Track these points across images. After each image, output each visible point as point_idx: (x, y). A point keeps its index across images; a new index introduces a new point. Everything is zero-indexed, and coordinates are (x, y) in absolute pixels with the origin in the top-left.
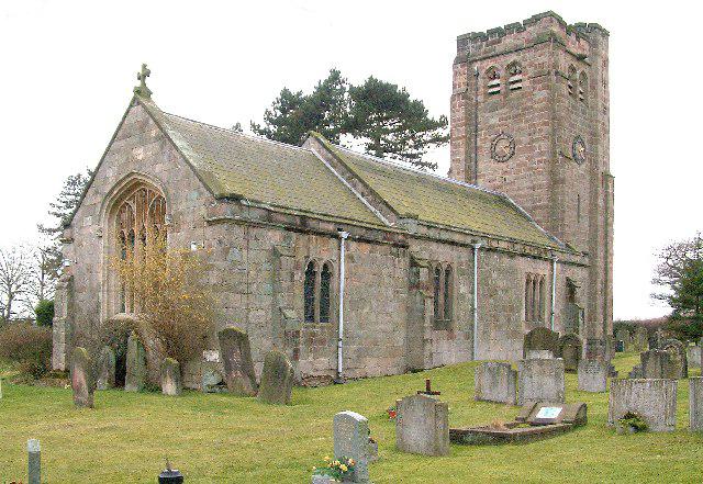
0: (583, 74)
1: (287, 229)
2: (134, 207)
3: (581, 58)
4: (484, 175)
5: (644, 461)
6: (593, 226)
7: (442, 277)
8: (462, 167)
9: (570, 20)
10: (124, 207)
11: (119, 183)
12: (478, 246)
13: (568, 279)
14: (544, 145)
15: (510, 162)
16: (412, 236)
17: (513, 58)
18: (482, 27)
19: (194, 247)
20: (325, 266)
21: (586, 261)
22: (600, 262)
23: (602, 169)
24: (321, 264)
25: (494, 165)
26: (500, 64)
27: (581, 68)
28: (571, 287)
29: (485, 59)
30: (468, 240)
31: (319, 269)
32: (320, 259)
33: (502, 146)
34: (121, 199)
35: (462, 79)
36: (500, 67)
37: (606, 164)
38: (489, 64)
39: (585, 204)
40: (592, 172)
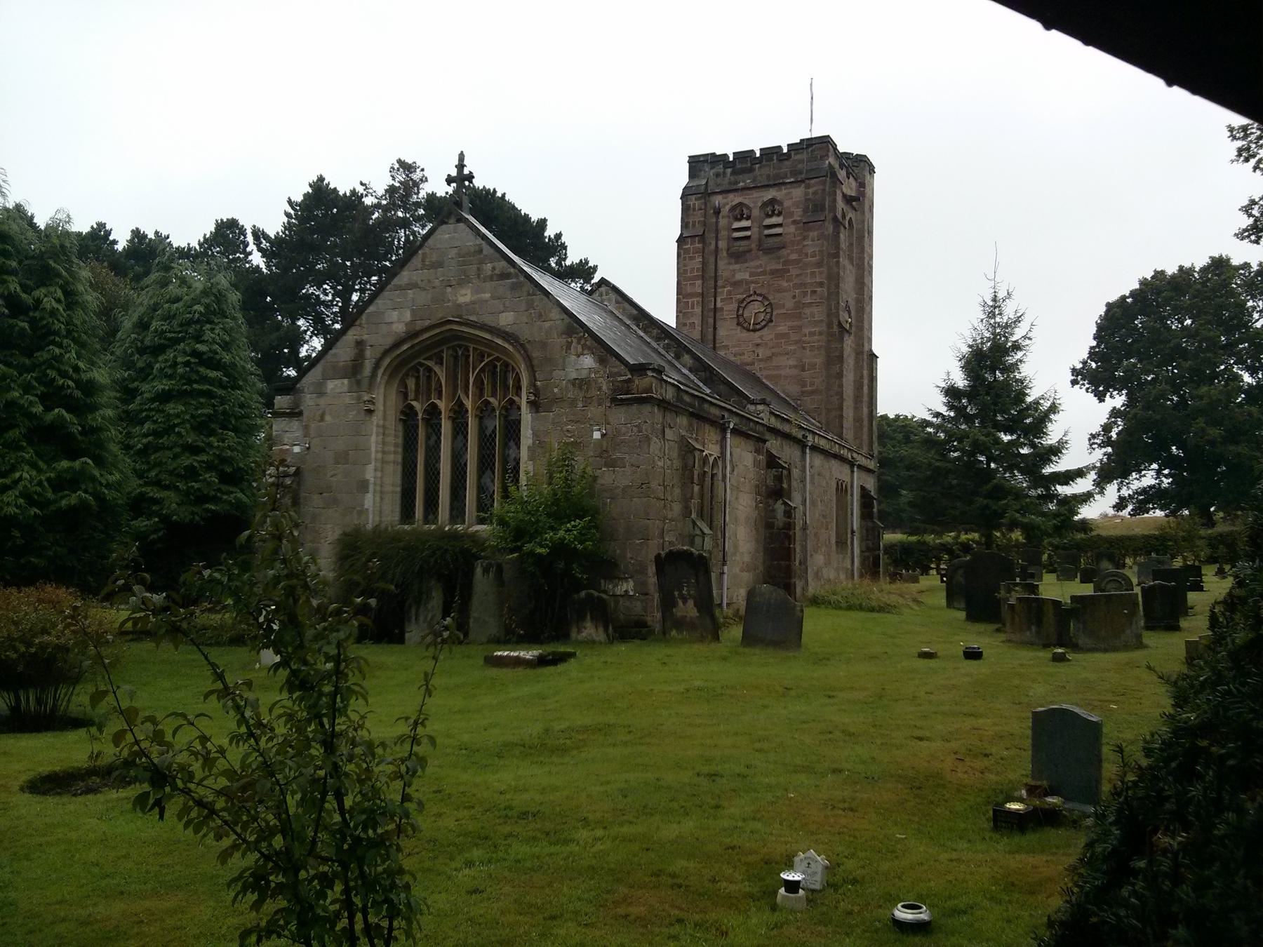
2: (441, 373)
5: (513, 734)
14: (818, 313)
18: (728, 146)
23: (866, 348)
26: (754, 200)
32: (711, 455)
33: (755, 310)
34: (414, 357)
35: (698, 217)
36: (751, 205)
38: (735, 199)
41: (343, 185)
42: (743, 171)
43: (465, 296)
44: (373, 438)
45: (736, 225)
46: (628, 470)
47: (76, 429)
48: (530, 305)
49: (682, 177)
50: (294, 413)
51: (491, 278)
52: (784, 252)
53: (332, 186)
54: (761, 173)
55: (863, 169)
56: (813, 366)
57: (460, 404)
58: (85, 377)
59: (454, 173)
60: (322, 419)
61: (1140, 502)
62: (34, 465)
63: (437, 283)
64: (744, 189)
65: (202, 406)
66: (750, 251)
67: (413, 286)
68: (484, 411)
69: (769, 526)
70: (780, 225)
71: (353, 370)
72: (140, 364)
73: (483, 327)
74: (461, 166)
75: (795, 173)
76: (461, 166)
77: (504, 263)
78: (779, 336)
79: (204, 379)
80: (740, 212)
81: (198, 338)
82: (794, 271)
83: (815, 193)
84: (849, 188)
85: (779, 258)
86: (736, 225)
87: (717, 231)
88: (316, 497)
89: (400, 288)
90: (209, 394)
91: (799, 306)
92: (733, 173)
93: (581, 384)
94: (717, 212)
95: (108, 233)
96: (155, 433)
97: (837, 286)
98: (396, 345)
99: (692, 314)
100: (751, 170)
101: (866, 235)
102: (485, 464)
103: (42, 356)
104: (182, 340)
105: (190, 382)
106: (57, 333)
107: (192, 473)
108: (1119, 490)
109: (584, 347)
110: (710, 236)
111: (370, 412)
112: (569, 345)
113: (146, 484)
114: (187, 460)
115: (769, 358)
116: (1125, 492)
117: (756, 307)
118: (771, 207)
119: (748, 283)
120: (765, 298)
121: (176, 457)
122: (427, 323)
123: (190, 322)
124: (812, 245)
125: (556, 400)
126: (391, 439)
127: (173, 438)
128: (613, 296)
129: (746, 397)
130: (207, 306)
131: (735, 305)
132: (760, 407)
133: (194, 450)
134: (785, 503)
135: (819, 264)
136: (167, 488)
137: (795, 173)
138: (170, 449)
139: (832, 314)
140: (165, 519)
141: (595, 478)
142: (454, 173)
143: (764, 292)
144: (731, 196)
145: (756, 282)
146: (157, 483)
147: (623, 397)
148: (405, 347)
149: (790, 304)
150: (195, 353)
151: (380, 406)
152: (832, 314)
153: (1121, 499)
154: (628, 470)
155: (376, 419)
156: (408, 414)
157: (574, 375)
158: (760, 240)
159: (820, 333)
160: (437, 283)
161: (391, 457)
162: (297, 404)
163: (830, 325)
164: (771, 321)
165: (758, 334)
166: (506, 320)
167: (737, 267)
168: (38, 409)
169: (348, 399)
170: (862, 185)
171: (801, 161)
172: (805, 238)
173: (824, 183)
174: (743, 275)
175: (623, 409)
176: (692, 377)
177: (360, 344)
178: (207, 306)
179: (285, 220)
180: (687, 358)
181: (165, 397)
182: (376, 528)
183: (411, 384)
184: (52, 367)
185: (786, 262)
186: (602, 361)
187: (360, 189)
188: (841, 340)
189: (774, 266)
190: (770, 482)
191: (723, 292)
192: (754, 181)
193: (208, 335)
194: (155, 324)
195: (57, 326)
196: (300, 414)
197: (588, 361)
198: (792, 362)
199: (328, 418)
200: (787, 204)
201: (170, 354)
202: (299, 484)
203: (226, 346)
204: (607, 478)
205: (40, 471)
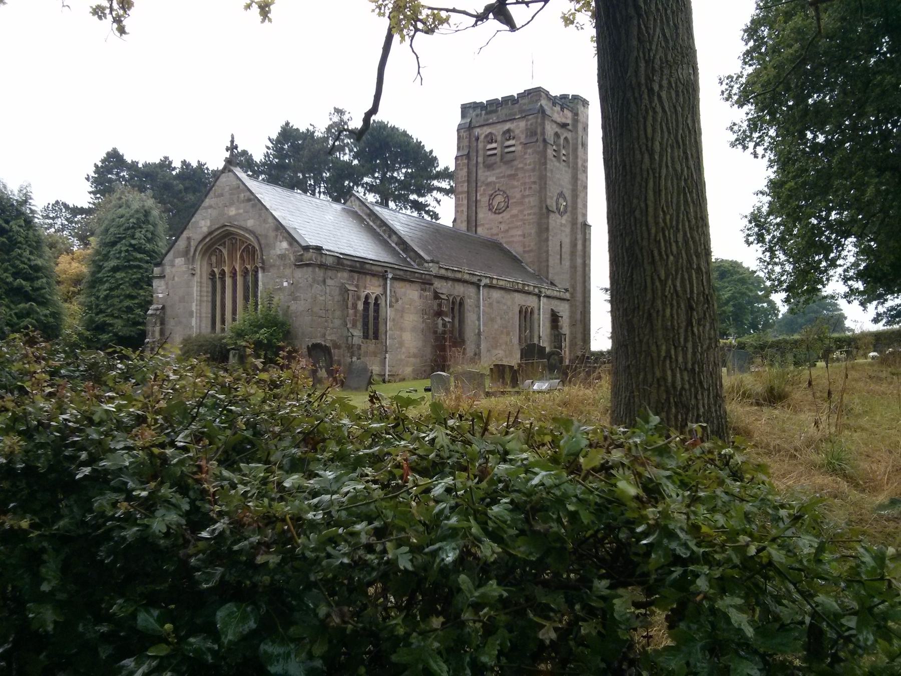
0: (566, 139)
1: (351, 271)
2: (225, 252)
3: (564, 126)
4: (483, 225)
6: (573, 267)
7: (456, 307)
8: (465, 217)
9: (555, 92)
10: (215, 251)
11: (210, 233)
12: (482, 284)
13: (552, 310)
14: (533, 201)
15: (504, 214)
16: (436, 276)
17: (507, 126)
18: (483, 98)
19: (285, 284)
20: (376, 299)
21: (567, 295)
22: (579, 296)
23: (580, 220)
24: (374, 296)
25: (491, 216)
27: (564, 134)
28: (555, 318)
29: (483, 126)
30: (475, 279)
31: (372, 301)
34: (214, 244)
35: (466, 142)
37: (585, 215)
38: (487, 130)
39: (566, 248)
40: (574, 223)
41: (302, 126)
42: (491, 112)
43: (232, 212)
44: (195, 288)
45: (490, 146)
46: (302, 302)
47: (29, 289)
48: (260, 216)
49: (456, 119)
50: (162, 277)
51: (243, 202)
52: (515, 163)
53: (295, 127)
54: (503, 112)
55: (577, 103)
56: (530, 234)
57: (234, 269)
58: (32, 263)
59: (229, 145)
60: (173, 279)
61: (892, 316)
62: (8, 307)
63: (220, 205)
64: (493, 123)
65: (135, 273)
66: (495, 163)
67: (210, 207)
68: (245, 273)
69: (435, 332)
70: (514, 145)
71: (186, 253)
72: (104, 252)
73: (240, 228)
74: (232, 142)
75: (521, 111)
76: (232, 142)
77: (248, 193)
78: (513, 216)
79: (136, 259)
80: (490, 139)
81: (133, 237)
82: (520, 175)
83: (531, 124)
84: (567, 117)
85: (512, 167)
86: (490, 146)
87: (477, 152)
88: (172, 320)
89: (206, 208)
90: (139, 267)
91: (524, 197)
92: (487, 114)
93: (282, 257)
94: (477, 139)
95: (171, 163)
96: (111, 289)
97: (545, 184)
98: (205, 238)
99: (462, 205)
100: (496, 111)
101: (580, 146)
102: (246, 298)
103: (14, 254)
104: (124, 238)
105: (128, 261)
106: (20, 242)
107: (129, 310)
108: (876, 308)
109: (283, 237)
110: (473, 154)
111: (193, 275)
112: (277, 235)
113: (107, 316)
114: (128, 303)
115: (507, 231)
116: (881, 309)
117: (499, 199)
118: (508, 134)
119: (495, 183)
120: (504, 192)
121: (121, 302)
122: (217, 226)
123: (128, 229)
124: (530, 158)
125: (272, 266)
126: (204, 289)
127: (119, 291)
128: (357, 202)
129: (424, 259)
130: (138, 219)
131: (487, 198)
132: (431, 265)
133: (131, 297)
134: (443, 320)
135: (533, 170)
136: (117, 317)
137: (521, 111)
138: (118, 297)
139: (542, 200)
140: (116, 334)
141: (289, 307)
142: (229, 145)
143: (503, 188)
144: (485, 128)
145: (499, 183)
146: (112, 315)
147: (301, 264)
148: (207, 240)
149: (518, 196)
150: (131, 245)
151: (198, 271)
152: (542, 200)
153: (878, 315)
154: (302, 302)
155: (196, 279)
156: (213, 274)
157: (279, 253)
158: (502, 155)
159: (535, 214)
160: (220, 205)
161: (205, 298)
162: (163, 271)
163: (541, 208)
164: (508, 207)
165: (501, 215)
166: (250, 223)
167: (488, 173)
168: (10, 279)
169: (184, 268)
170: (576, 114)
171: (525, 104)
172: (525, 153)
173: (537, 118)
174: (492, 179)
175: (300, 270)
176: (397, 248)
177: (189, 239)
178: (138, 219)
179: (266, 150)
180: (394, 237)
181: (115, 269)
182: (199, 335)
183: (214, 259)
184: (18, 259)
185: (517, 169)
186: (290, 244)
187: (311, 128)
188: (548, 217)
189: (509, 172)
190: (435, 308)
191: (481, 189)
192: (498, 118)
193: (137, 235)
194: (112, 230)
195: (20, 239)
196: (164, 277)
197: (285, 245)
198: (520, 233)
199: (176, 279)
200: (517, 132)
201: (118, 246)
202: (164, 314)
203: (149, 240)
204: (294, 307)
205: (11, 309)
